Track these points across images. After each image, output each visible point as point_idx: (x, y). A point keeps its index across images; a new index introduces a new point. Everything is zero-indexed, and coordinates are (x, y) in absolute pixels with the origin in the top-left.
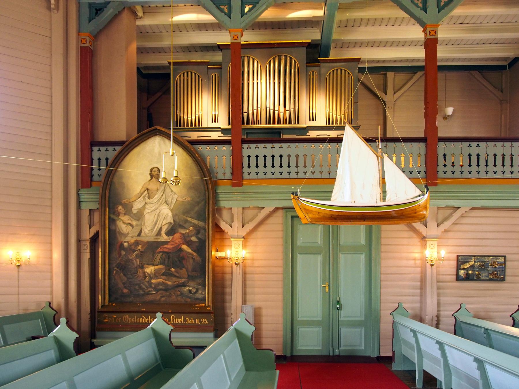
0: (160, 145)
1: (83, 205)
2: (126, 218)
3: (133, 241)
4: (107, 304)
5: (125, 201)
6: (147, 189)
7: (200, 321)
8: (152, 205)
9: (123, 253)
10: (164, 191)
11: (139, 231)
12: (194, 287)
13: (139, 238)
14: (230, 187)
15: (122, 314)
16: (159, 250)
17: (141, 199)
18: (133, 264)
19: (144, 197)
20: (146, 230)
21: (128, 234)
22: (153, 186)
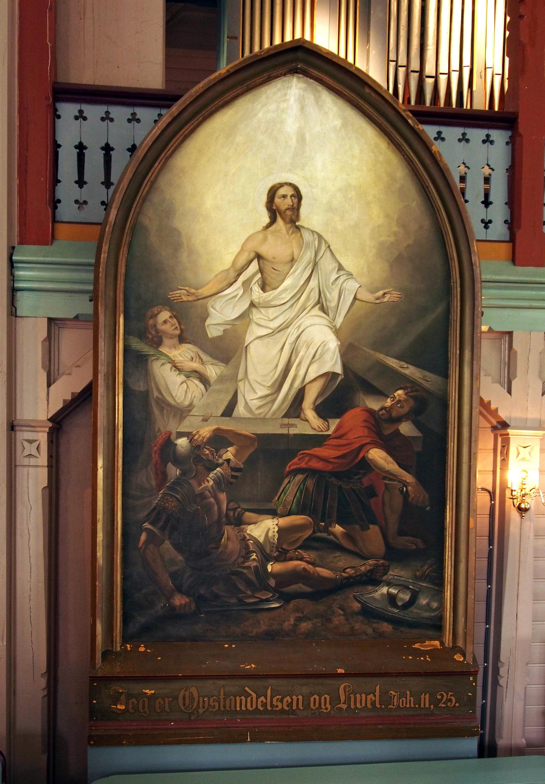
0: (302, 108)
1: (25, 302)
2: (184, 354)
3: (206, 431)
4: (118, 648)
5: (181, 294)
6: (259, 257)
7: (435, 702)
8: (272, 312)
9: (174, 472)
10: (315, 264)
11: (229, 397)
12: (404, 587)
13: (227, 425)
14: (507, 265)
15: (175, 685)
16: (294, 463)
17: (237, 288)
18: (208, 509)
19: (246, 284)
20: (250, 396)
21: (191, 406)
22: (277, 246)
